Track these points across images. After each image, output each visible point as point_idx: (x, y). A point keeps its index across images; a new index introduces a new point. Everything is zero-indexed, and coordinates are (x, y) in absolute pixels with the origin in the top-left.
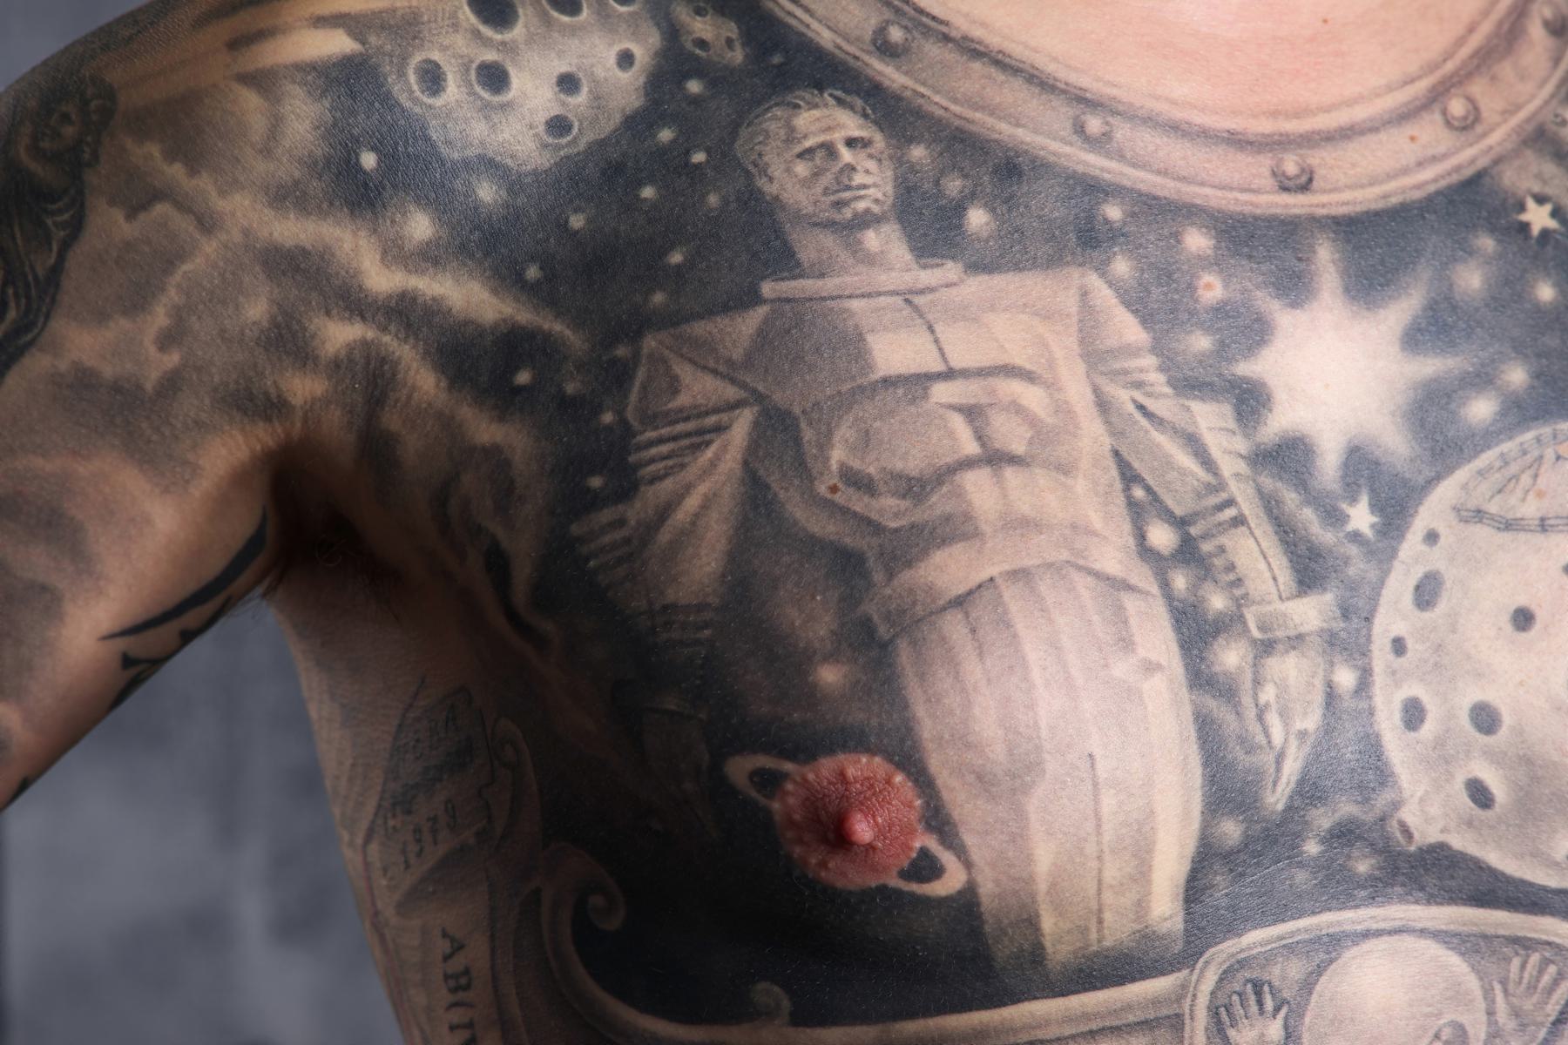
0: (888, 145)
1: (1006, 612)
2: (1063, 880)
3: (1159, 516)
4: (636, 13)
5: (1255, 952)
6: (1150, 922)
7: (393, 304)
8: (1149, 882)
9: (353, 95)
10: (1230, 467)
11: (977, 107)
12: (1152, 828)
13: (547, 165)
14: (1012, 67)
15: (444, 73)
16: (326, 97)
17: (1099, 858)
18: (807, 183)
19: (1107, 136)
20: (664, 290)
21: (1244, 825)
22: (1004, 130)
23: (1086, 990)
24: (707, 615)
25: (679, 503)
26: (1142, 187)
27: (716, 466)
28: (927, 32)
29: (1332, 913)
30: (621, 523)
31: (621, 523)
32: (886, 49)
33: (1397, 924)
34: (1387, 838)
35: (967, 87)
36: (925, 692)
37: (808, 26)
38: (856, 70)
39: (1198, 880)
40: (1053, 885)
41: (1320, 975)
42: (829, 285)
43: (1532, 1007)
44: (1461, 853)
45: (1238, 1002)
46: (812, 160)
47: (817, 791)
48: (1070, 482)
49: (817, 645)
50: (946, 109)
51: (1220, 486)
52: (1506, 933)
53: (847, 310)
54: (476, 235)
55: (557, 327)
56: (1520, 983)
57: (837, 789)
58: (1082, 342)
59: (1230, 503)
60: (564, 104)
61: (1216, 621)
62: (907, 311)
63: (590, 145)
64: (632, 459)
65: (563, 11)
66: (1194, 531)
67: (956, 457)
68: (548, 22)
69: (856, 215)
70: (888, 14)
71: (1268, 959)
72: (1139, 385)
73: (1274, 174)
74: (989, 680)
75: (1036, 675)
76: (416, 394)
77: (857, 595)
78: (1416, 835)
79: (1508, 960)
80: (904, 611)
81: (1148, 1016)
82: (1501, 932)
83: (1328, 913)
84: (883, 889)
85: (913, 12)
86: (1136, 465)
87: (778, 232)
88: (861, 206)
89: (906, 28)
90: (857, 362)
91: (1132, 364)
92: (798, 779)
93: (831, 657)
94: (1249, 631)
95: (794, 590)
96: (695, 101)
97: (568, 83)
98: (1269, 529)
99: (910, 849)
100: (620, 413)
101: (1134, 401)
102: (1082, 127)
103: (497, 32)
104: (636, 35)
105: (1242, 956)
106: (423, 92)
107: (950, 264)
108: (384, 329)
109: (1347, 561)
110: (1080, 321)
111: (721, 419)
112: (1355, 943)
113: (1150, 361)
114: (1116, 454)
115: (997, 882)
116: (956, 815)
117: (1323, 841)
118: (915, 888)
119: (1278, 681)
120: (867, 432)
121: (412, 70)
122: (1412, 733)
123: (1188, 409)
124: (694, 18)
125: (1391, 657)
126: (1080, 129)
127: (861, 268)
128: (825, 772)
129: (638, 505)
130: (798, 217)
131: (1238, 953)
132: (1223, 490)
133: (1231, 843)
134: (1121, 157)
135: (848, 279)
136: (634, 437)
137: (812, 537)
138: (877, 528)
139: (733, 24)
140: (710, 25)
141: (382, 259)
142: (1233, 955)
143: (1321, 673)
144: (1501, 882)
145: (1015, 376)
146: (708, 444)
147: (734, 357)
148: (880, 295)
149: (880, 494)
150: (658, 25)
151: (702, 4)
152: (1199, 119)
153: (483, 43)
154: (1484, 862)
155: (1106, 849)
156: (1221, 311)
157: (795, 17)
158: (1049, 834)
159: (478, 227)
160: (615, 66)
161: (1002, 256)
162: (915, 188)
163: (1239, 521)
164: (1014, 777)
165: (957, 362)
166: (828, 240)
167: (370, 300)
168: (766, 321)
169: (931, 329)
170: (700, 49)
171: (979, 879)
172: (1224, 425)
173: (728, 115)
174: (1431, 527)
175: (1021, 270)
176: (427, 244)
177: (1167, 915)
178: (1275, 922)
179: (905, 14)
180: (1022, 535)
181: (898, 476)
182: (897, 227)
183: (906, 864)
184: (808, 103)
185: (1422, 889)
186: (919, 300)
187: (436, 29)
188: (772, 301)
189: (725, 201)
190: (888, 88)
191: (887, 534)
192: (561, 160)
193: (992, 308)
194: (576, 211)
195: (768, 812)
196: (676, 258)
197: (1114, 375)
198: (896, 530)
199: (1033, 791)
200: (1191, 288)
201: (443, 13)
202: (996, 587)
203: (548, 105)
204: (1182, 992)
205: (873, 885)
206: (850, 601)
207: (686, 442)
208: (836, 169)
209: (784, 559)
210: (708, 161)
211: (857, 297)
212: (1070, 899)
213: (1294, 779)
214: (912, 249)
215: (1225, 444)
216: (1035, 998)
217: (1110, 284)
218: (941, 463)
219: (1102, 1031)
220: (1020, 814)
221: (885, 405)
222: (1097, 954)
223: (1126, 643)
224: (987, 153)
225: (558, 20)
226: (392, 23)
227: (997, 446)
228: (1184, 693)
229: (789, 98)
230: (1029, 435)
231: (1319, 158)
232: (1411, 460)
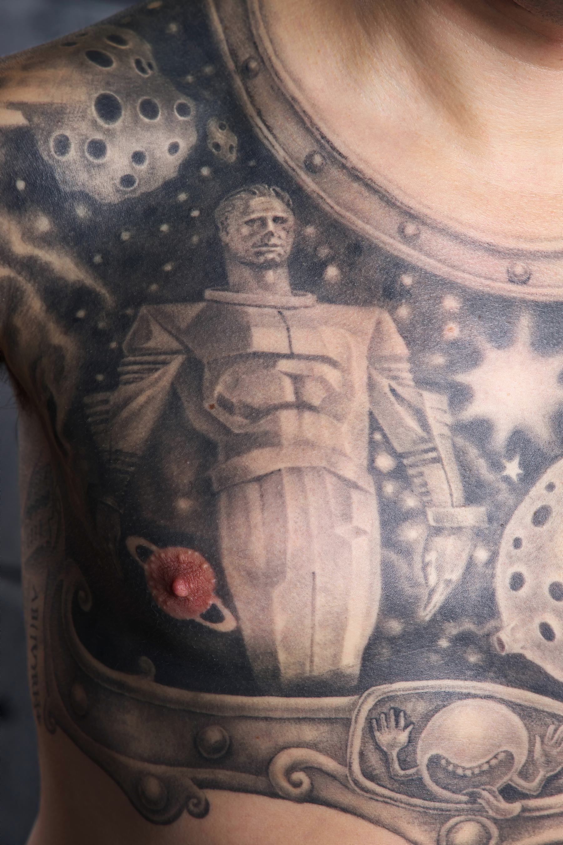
0: (295, 224)
1: (282, 488)
2: (291, 636)
3: (386, 451)
4: (188, 122)
5: (399, 693)
6: (340, 667)
7: (25, 261)
8: (342, 646)
9: (18, 149)
10: (437, 429)
11: (348, 209)
12: (346, 618)
13: (116, 202)
15: (70, 144)
16: (4, 147)
17: (312, 628)
18: (245, 239)
19: (417, 236)
21: (404, 625)
22: (360, 224)
23: (299, 696)
24: (134, 460)
28: (334, 161)
29: (450, 680)
30: (106, 402)
31: (106, 402)
32: (310, 168)
33: (487, 693)
34: (490, 646)
35: (347, 197)
37: (273, 146)
39: (371, 649)
40: (285, 638)
42: (241, 297)
44: (531, 662)
46: (252, 226)
47: (165, 563)
48: (339, 425)
49: (181, 487)
50: (332, 207)
51: (431, 439)
53: (246, 312)
54: (72, 233)
55: (103, 291)
56: (552, 739)
58: (370, 349)
59: (434, 449)
60: (133, 168)
61: (407, 513)
62: (278, 318)
63: (142, 194)
64: (120, 369)
65: (146, 115)
67: (281, 401)
68: (136, 121)
69: (266, 261)
70: (316, 148)
71: (407, 698)
72: (395, 378)
74: (264, 523)
75: (291, 525)
76: (30, 310)
77: (208, 465)
78: (507, 647)
80: (229, 478)
81: (331, 717)
82: (546, 709)
83: (447, 680)
84: (192, 622)
85: (330, 148)
86: (380, 421)
88: (270, 256)
89: (324, 157)
90: (243, 341)
91: (393, 366)
92: (157, 555)
93: (187, 495)
94: (428, 521)
95: (178, 456)
96: (203, 180)
97: (138, 157)
98: (456, 467)
99: (207, 604)
100: (120, 344)
101: (390, 386)
102: (403, 229)
103: (106, 123)
104: (184, 136)
105: (391, 694)
106: (56, 153)
107: (310, 295)
108: (20, 274)
109: (498, 491)
110: (372, 338)
111: (166, 358)
113: (406, 366)
114: (371, 414)
115: (253, 631)
116: (232, 591)
117: (451, 640)
118: (208, 624)
120: (237, 380)
122: (514, 592)
124: (218, 130)
125: (512, 548)
126: (401, 230)
128: (170, 555)
129: (116, 394)
130: (235, 256)
131: (388, 692)
132: (430, 442)
135: (251, 296)
136: (123, 358)
137: (194, 429)
138: (227, 431)
139: (236, 138)
140: (224, 136)
142: (385, 693)
143: (467, 550)
144: (551, 682)
146: (157, 370)
147: (182, 326)
148: (265, 307)
149: (235, 414)
150: (198, 131)
151: (224, 123)
152: (473, 234)
153: (96, 128)
154: (543, 669)
155: (317, 624)
156: (454, 344)
157: (268, 140)
158: (283, 610)
159: (74, 229)
160: (167, 151)
162: (302, 250)
163: (437, 460)
164: (267, 577)
165: (298, 348)
166: (247, 273)
167: (14, 257)
168: (203, 311)
169: (288, 329)
170: (215, 149)
171: (243, 627)
174: (552, 481)
175: (348, 304)
176: (46, 234)
177: (351, 665)
178: (413, 680)
179: (325, 149)
180: (303, 450)
181: (247, 406)
182: (286, 270)
183: (204, 611)
184: (260, 192)
185: (505, 677)
186: (287, 313)
187: (72, 118)
188: (208, 301)
189: (201, 241)
191: (232, 436)
192: (125, 200)
193: (326, 323)
194: (127, 230)
195: (142, 569)
196: (168, 267)
198: (237, 435)
199: (277, 586)
200: (440, 329)
201: (79, 109)
202: (281, 475)
203: (125, 168)
205: (188, 619)
207: (146, 366)
209: (177, 438)
210: (199, 217)
212: (295, 647)
213: (438, 605)
214: (291, 285)
215: (438, 417)
216: (272, 695)
217: (395, 320)
219: (304, 719)
220: (269, 598)
222: (308, 678)
223: (347, 517)
224: (346, 236)
225: (142, 120)
227: (305, 399)
228: (378, 549)
229: (252, 188)
230: (324, 396)
231: (536, 267)
232: (549, 443)
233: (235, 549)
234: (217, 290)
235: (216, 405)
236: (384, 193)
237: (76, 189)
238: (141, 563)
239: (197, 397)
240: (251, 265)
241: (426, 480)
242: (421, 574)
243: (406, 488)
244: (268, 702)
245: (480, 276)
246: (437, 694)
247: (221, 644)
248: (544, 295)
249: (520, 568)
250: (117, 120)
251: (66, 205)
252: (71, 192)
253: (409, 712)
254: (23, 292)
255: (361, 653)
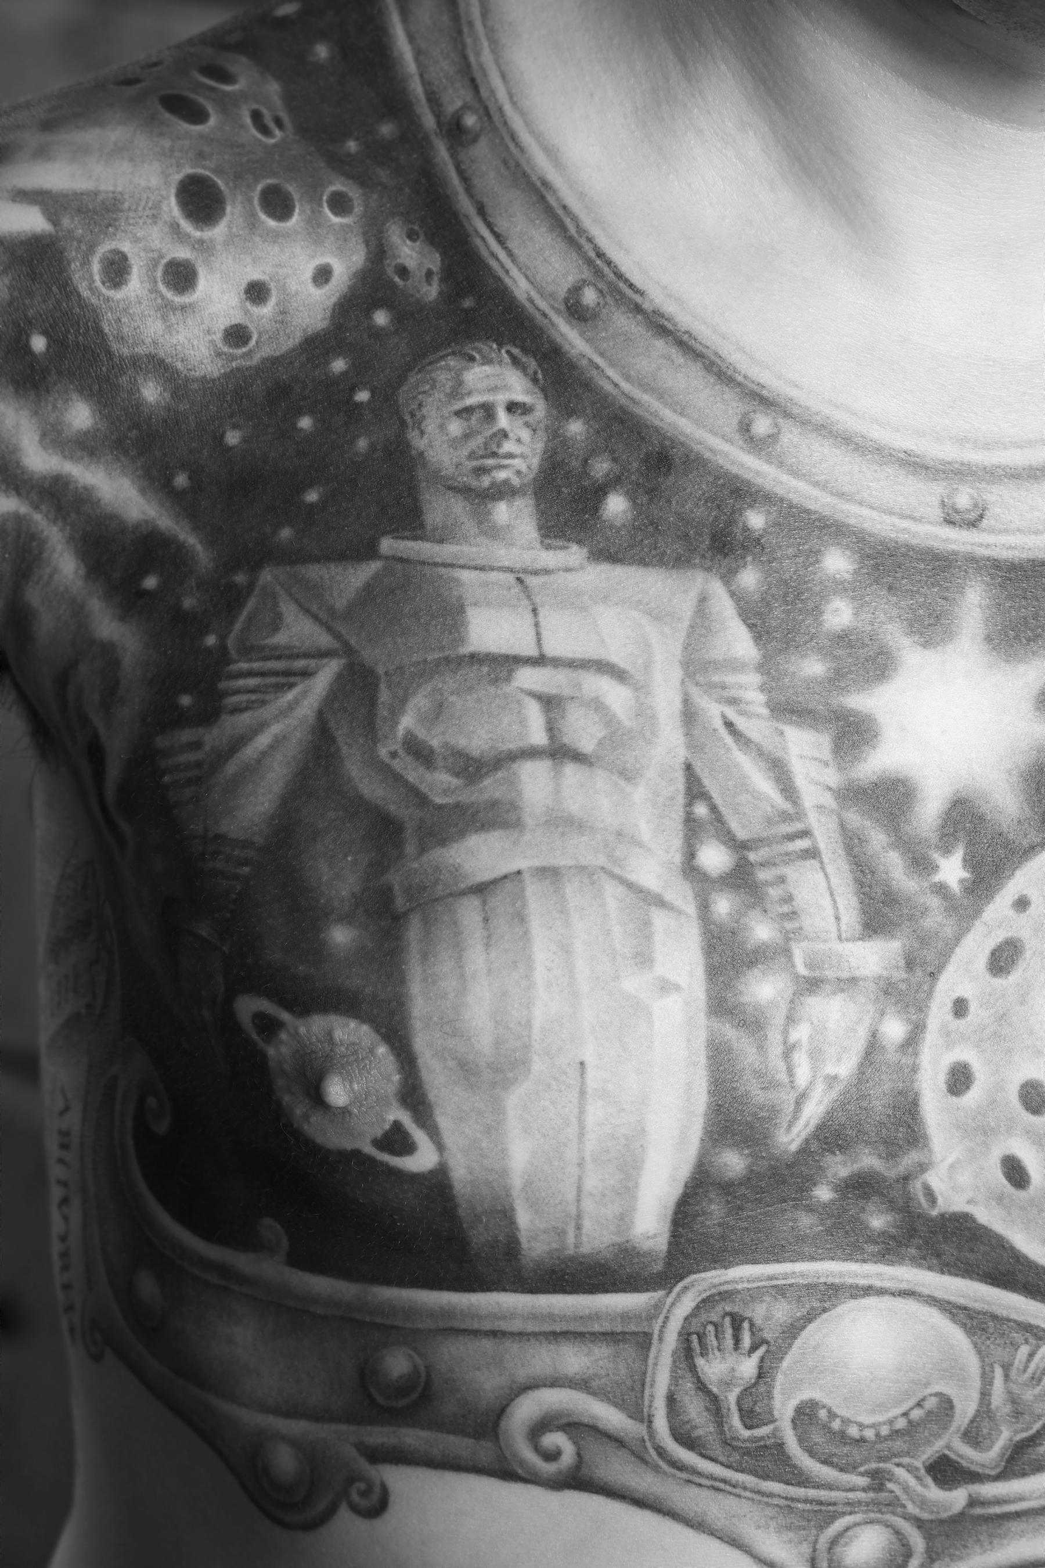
0: (549, 414)
1: (524, 905)
2: (540, 1180)
4: (348, 226)
5: (740, 1287)
8: (634, 1198)
9: (33, 276)
10: (811, 796)
11: (646, 388)
13: (216, 374)
14: (694, 351)
15: (130, 267)
16: (7, 274)
17: (580, 1165)
18: (455, 443)
19: (773, 438)
20: (293, 526)
21: (750, 1159)
25: (251, 739)
26: (795, 499)
27: (292, 709)
28: (621, 299)
29: (834, 1262)
32: (576, 311)
33: (904, 1286)
34: (909, 1198)
35: (644, 365)
36: (425, 970)
37: (507, 272)
38: (541, 329)
39: (689, 1205)
40: (528, 1183)
41: (810, 1321)
42: (446, 551)
43: (1031, 1398)
44: (986, 1228)
45: (713, 1333)
46: (468, 420)
47: (306, 1045)
48: (629, 788)
49: (336, 904)
50: (616, 385)
51: (799, 815)
52: (1020, 1318)
53: (457, 580)
54: (134, 433)
56: (1025, 1371)
57: (323, 1047)
58: (686, 647)
59: (805, 833)
60: (247, 312)
61: (756, 951)
62: (517, 589)
63: (264, 360)
64: (222, 685)
66: (752, 856)
67: (521, 744)
68: (253, 224)
71: (755, 1295)
72: (733, 702)
73: (943, 503)
74: (490, 970)
75: (540, 975)
76: (56, 576)
78: (940, 1201)
79: (1016, 1347)
80: (426, 888)
81: (615, 1329)
82: (1014, 1316)
83: (830, 1262)
84: (357, 1153)
85: (612, 275)
86: (706, 782)
87: (413, 491)
88: (502, 475)
89: (601, 291)
90: (450, 633)
91: (730, 679)
92: (292, 1030)
93: (346, 919)
94: (793, 966)
96: (377, 334)
97: (256, 292)
99: (384, 1120)
100: (223, 638)
101: (723, 716)
102: (748, 425)
103: (197, 228)
105: (725, 1288)
106: (103, 283)
107: (575, 548)
108: (36, 507)
109: (925, 911)
110: (691, 627)
111: (309, 665)
112: (854, 1297)
113: (753, 679)
114: (688, 767)
116: (431, 1096)
117: (836, 1188)
119: (815, 1022)
120: (441, 705)
121: (98, 259)
122: (954, 1098)
123: (782, 733)
124: (404, 242)
125: (950, 1017)
126: (745, 428)
127: (481, 539)
128: (315, 1029)
129: (215, 731)
130: (436, 476)
131: (720, 1284)
132: (799, 820)
133: (731, 1174)
134: (781, 464)
135: (466, 549)
136: (228, 664)
137: (361, 797)
138: (421, 800)
139: (438, 255)
140: (416, 252)
141: (41, 441)
142: (715, 1286)
143: (867, 1022)
144: (1023, 1265)
145: (606, 672)
146: (291, 686)
147: (338, 606)
148: (493, 570)
149: (436, 768)
150: (367, 243)
151: (416, 228)
153: (179, 238)
155: (588, 1159)
156: (843, 638)
157: (497, 259)
160: (310, 281)
161: (631, 547)
162: (561, 464)
163: (812, 854)
164: (496, 1070)
165: (553, 647)
166: (458, 507)
167: (26, 477)
168: (376, 577)
169: (535, 611)
170: (399, 277)
171: (452, 1163)
172: (818, 755)
173: (403, 355)
174: (1025, 892)
177: (651, 1234)
178: (767, 1261)
184: (483, 357)
185: (938, 1256)
186: (532, 581)
187: (134, 218)
188: (387, 558)
189: (372, 447)
190: (567, 352)
191: (431, 808)
193: (605, 599)
194: (235, 427)
195: (264, 1057)
196: (312, 496)
197: (710, 687)
198: (440, 807)
200: (817, 612)
202: (521, 881)
203: (232, 312)
204: (653, 1313)
205: (349, 1148)
206: (379, 867)
207: (272, 680)
208: (488, 433)
210: (369, 402)
211: (469, 568)
212: (547, 1200)
213: (814, 1122)
214: (540, 528)
216: (505, 1290)
217: (733, 594)
218: (504, 748)
219: (565, 1334)
220: (498, 1107)
221: (465, 680)
222: (572, 1259)
223: (644, 959)
226: (91, 207)
227: (566, 740)
228: (702, 1019)
233: (435, 1019)
234: (403, 538)
235: (401, 752)
236: (713, 357)
237: (141, 350)
238: (261, 1044)
239: (366, 736)
240: (465, 491)
241: (792, 890)
242: (782, 1066)
243: (752, 906)
244: (498, 1303)
245: (891, 513)
246: (811, 1287)
247: (410, 1194)
248: (1010, 548)
249: (964, 1054)
250: (217, 222)
251: (123, 380)
252: (132, 356)
253: (758, 1322)
254: (43, 542)
255: (670, 1212)
